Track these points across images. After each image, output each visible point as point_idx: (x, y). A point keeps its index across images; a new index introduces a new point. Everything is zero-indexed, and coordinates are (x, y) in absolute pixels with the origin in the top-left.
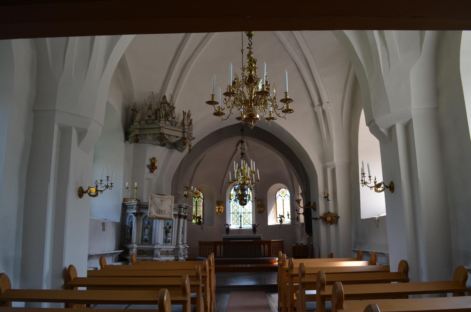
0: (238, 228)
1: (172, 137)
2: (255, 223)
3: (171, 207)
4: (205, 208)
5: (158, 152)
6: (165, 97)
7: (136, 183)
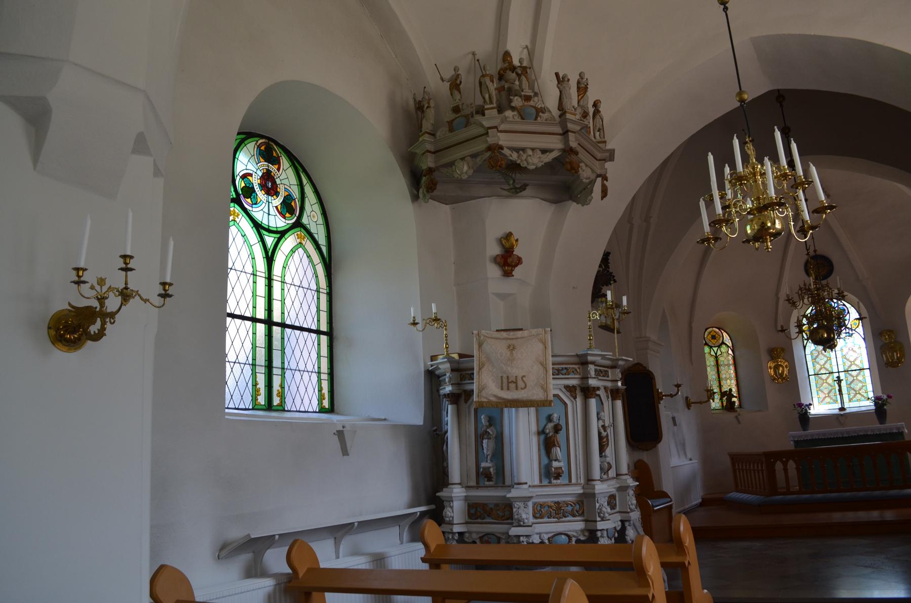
0: (837, 412)
1: (530, 152)
2: (880, 394)
3: (544, 365)
4: (739, 370)
5: (521, 216)
6: (507, 54)
7: (433, 305)
